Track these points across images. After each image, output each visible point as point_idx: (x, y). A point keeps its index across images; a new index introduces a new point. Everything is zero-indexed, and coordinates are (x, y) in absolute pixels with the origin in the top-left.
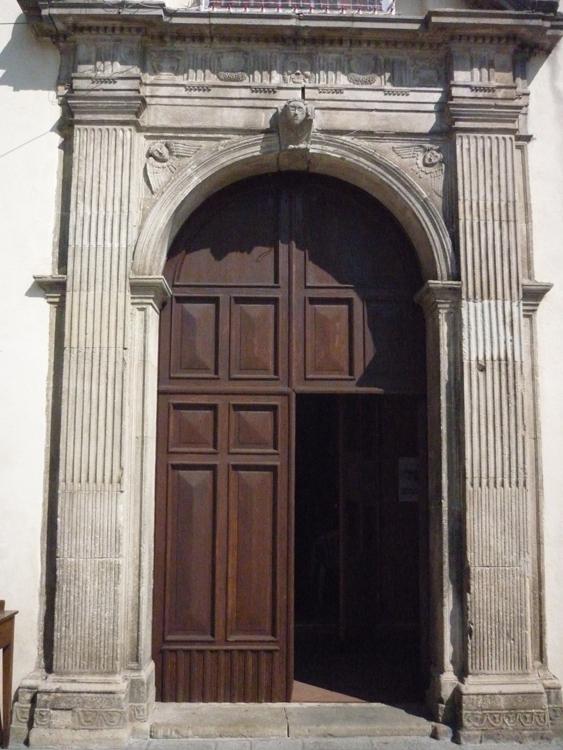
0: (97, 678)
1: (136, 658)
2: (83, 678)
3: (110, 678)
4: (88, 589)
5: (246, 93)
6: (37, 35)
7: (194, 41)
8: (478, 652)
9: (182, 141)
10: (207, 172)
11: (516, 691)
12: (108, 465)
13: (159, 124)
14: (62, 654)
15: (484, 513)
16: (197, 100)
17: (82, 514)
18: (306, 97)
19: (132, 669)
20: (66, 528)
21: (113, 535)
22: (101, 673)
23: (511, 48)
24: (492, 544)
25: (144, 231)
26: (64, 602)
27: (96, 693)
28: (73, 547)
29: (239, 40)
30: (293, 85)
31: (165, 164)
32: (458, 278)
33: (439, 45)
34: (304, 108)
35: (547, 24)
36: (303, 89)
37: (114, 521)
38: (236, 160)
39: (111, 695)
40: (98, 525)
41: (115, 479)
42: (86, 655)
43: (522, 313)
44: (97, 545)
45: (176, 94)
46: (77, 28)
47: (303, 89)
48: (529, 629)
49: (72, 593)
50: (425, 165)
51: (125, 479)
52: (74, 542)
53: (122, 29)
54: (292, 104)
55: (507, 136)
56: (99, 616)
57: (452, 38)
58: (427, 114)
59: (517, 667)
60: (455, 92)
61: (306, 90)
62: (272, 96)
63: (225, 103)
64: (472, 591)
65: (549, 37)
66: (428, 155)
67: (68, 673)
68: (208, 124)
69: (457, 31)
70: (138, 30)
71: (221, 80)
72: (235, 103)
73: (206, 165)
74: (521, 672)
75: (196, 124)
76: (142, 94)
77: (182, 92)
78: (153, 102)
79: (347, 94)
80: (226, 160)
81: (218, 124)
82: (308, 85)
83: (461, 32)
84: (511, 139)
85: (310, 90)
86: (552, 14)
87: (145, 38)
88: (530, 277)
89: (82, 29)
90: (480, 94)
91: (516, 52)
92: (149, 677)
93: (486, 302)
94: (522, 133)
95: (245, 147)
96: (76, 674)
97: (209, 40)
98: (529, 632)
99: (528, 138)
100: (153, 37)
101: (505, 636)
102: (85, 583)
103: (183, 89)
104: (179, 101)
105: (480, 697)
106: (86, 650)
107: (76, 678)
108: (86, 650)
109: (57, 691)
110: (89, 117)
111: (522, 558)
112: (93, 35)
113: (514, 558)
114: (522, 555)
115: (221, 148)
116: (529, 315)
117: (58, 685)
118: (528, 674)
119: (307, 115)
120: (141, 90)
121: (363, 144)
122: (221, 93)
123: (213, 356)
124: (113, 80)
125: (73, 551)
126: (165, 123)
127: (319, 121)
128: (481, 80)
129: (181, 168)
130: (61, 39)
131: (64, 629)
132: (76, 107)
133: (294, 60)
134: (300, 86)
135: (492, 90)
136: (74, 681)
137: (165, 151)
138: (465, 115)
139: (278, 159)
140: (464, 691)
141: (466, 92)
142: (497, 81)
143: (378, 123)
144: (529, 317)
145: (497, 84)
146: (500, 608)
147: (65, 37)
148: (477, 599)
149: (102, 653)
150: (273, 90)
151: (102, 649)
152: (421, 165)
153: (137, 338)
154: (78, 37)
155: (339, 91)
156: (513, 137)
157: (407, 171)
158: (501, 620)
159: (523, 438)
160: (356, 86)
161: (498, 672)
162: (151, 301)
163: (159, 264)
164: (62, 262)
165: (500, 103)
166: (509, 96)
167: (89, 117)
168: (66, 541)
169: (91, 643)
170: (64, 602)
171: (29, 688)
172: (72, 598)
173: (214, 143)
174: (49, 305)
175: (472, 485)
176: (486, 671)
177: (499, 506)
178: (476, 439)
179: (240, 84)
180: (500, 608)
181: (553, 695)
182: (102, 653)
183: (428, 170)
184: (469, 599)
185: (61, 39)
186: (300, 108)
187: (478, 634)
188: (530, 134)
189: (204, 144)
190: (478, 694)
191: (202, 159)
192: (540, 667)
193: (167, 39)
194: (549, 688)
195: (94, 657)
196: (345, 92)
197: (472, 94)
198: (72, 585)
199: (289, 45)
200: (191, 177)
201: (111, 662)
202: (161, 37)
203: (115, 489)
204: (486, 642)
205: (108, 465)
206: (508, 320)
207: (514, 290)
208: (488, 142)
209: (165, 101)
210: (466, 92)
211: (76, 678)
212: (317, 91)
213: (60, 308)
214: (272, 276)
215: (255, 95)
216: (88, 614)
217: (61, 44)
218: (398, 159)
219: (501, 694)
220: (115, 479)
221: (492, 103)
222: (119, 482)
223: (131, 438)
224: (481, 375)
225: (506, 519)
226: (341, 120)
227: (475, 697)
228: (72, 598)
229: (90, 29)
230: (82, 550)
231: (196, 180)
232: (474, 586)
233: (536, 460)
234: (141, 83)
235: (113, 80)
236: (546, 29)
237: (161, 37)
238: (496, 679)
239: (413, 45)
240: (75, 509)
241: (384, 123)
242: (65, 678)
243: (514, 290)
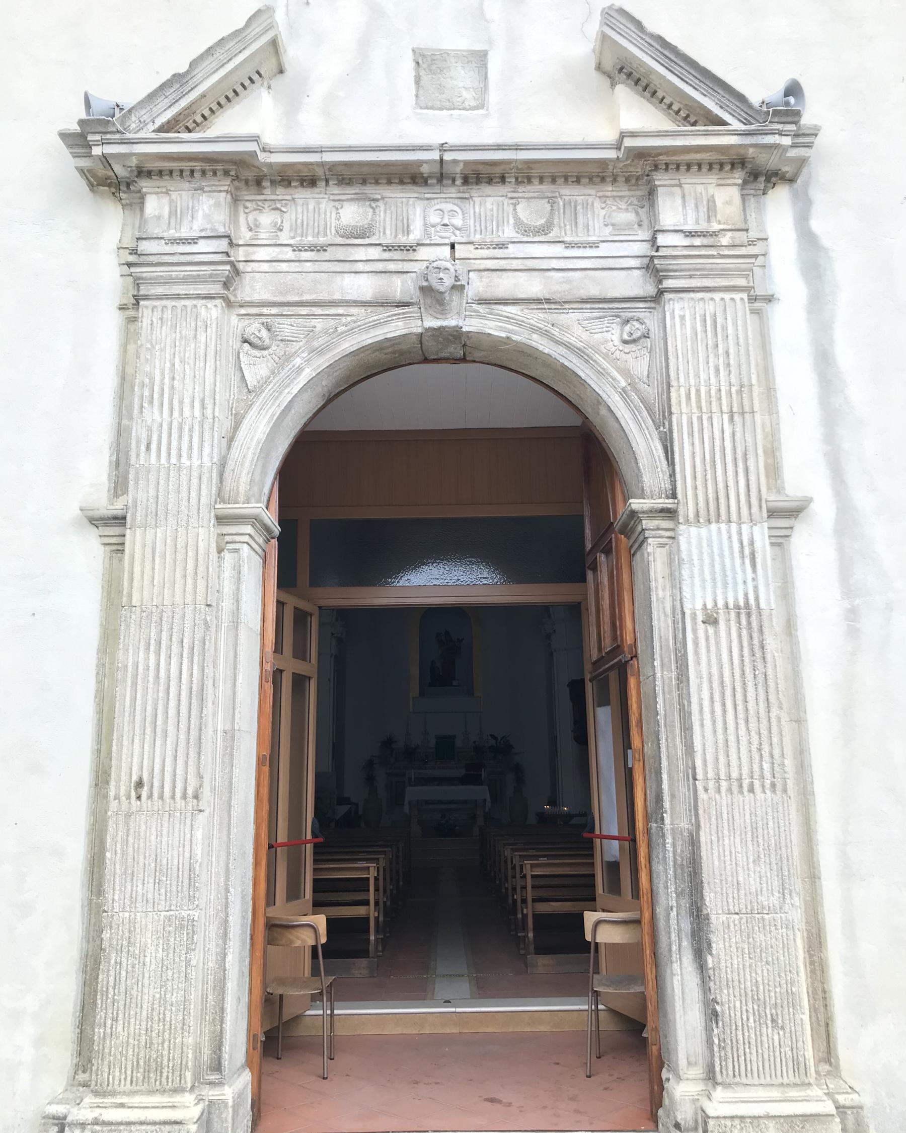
0: (157, 1099)
1: (217, 1067)
2: (137, 1100)
3: (177, 1099)
4: (148, 960)
5: (374, 253)
6: (91, 186)
7: (302, 185)
8: (729, 1049)
9: (289, 321)
10: (323, 362)
11: (791, 1113)
12: (180, 771)
13: (256, 297)
14: (106, 1063)
15: (726, 832)
16: (308, 264)
17: (142, 845)
18: (457, 256)
19: (212, 1084)
20: (118, 867)
21: (186, 875)
22: (163, 1092)
23: (738, 177)
24: (741, 879)
25: (236, 444)
26: (111, 979)
27: (154, 1123)
28: (128, 896)
29: (364, 182)
30: (439, 241)
31: (265, 353)
32: (674, 496)
33: (638, 179)
34: (452, 270)
35: (787, 141)
36: (453, 246)
37: (187, 855)
38: (364, 344)
39: (176, 1127)
40: (165, 861)
41: (190, 792)
42: (141, 1063)
43: (767, 542)
44: (163, 891)
45: (280, 257)
46: (143, 173)
47: (453, 246)
48: (807, 1012)
49: (124, 964)
50: (625, 342)
51: (206, 792)
52: (129, 888)
53: (204, 173)
54: (435, 264)
55: (737, 296)
56: (163, 1001)
57: (656, 167)
58: (624, 273)
59: (791, 1072)
60: (662, 240)
61: (457, 246)
62: (411, 255)
63: (347, 267)
64: (714, 952)
65: (792, 160)
66: (627, 328)
67: (114, 1094)
68: (323, 296)
69: (661, 157)
70: (226, 173)
71: (342, 237)
72: (360, 267)
73: (320, 352)
74: (798, 1081)
75: (306, 297)
76: (232, 259)
77: (289, 254)
78: (249, 270)
79: (512, 250)
80: (349, 345)
81: (337, 296)
82: (458, 239)
83: (664, 158)
84: (742, 299)
85: (462, 246)
86: (793, 127)
87: (236, 183)
88: (780, 490)
89: (149, 174)
90: (697, 242)
91: (745, 182)
92: (240, 1096)
93: (734, 526)
94: (759, 292)
95: (374, 326)
96: (124, 1093)
97: (323, 184)
98: (806, 1018)
99: (769, 299)
100: (247, 182)
101: (769, 1022)
102: (143, 950)
103: (289, 249)
104: (284, 266)
105: (737, 1122)
106: (142, 1055)
107: (125, 1100)
108: (142, 1055)
109: (96, 1122)
110: (160, 290)
111: (788, 901)
112: (166, 182)
113: (775, 900)
114: (787, 896)
115: (341, 329)
116: (780, 541)
117: (96, 1113)
118: (809, 1084)
119: (457, 278)
120: (232, 253)
121: (535, 317)
122: (341, 254)
123: (600, 267)
124: (193, 241)
125: (127, 902)
126: (266, 296)
127: (477, 286)
128: (697, 223)
129: (288, 358)
130: (123, 188)
131: (109, 1022)
132: (142, 279)
133: (438, 207)
134: (447, 241)
135: (714, 234)
136: (122, 1105)
137: (264, 333)
138: (676, 271)
139: (421, 343)
140: (711, 1113)
141: (678, 240)
142: (719, 223)
143: (556, 288)
144: (779, 545)
145: (721, 227)
146: (760, 979)
147: (128, 185)
148: (723, 964)
149: (166, 1059)
150: (412, 248)
151: (165, 1053)
152: (617, 342)
153: (226, 590)
154: (145, 185)
155: (502, 246)
156: (745, 296)
157: (598, 351)
158: (761, 997)
159: (779, 720)
160: (525, 239)
161: (762, 1081)
162: (246, 538)
163: (261, 491)
164: (119, 486)
165: (726, 252)
166: (737, 242)
167: (160, 290)
168: (117, 888)
169: (149, 1045)
170: (111, 979)
171: (54, 1118)
172: (123, 973)
173: (331, 323)
174: (102, 547)
175: (706, 790)
176: (744, 1080)
177: (748, 821)
178: (708, 722)
179: (367, 241)
180: (760, 979)
181: (851, 1120)
182: (166, 1059)
183: (627, 348)
184: (710, 965)
185: (123, 188)
186: (446, 269)
187: (727, 1020)
188: (770, 293)
189: (319, 324)
190: (732, 1118)
191: (316, 344)
192: (829, 1073)
193: (266, 184)
194: (844, 1107)
195: (153, 1065)
196: (510, 246)
197: (686, 242)
198: (124, 954)
199: (432, 185)
200: (300, 370)
201: (177, 1073)
202: (258, 182)
203: (190, 808)
204: (740, 1033)
205: (180, 771)
206: (747, 551)
207: (755, 509)
208: (711, 304)
209: (265, 267)
210: (678, 240)
211: (125, 1100)
212: (471, 247)
213: (118, 548)
214: (462, 257)
215: (387, 255)
216: (146, 997)
217: (123, 195)
218: (585, 336)
219: (769, 1117)
220: (190, 792)
221: (714, 252)
222: (196, 797)
223: (215, 732)
224: (711, 630)
225: (760, 840)
226: (505, 285)
227: (728, 1123)
228: (123, 973)
229: (160, 173)
230: (139, 899)
231: (308, 373)
232: (718, 944)
233: (801, 752)
234: (231, 244)
235: (193, 241)
236: (785, 149)
237: (258, 182)
238: (762, 1093)
239: (603, 180)
240: (131, 839)
241: (566, 287)
242: (109, 1100)
243: (755, 509)
